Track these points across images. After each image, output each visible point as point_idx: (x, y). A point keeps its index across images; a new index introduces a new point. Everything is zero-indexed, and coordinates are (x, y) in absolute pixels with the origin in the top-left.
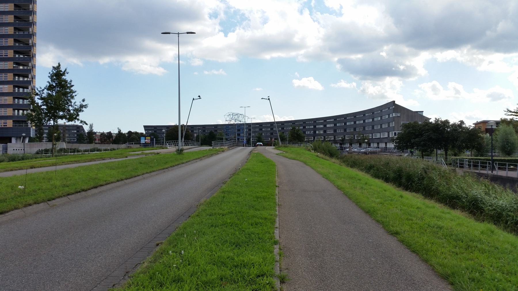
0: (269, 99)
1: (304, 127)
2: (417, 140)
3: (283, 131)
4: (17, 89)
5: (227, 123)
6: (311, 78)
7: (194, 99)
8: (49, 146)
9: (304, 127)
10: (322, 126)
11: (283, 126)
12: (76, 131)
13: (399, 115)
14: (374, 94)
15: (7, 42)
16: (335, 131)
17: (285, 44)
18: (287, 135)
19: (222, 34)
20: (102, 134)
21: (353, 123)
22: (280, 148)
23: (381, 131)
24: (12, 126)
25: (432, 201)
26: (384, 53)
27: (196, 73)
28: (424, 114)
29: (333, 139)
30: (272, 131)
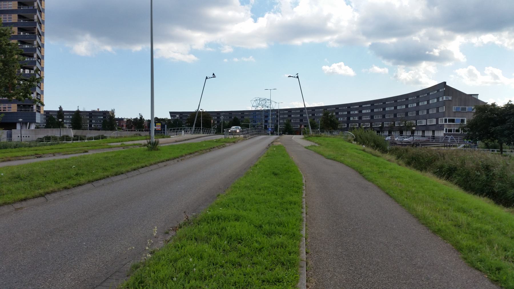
0: (298, 77)
1: (337, 113)
2: (499, 128)
3: (313, 117)
4: (22, 70)
5: (254, 109)
6: (342, 63)
7: (207, 78)
8: (72, 133)
9: (337, 113)
10: (356, 112)
12: (102, 117)
13: (450, 98)
15: (11, 18)
16: (372, 117)
17: (317, 29)
18: (318, 121)
19: (251, 20)
20: (129, 121)
21: (393, 108)
22: (310, 138)
23: (428, 116)
24: (16, 111)
25: (482, 199)
26: (418, 38)
27: (226, 60)
28: (480, 98)
29: (369, 126)
30: (301, 118)
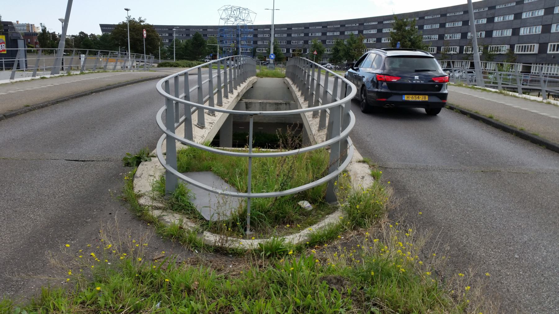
3: (307, 38)
5: (222, 23)
10: (374, 31)
11: (306, 31)
14: (306, 238)
30: (289, 39)
